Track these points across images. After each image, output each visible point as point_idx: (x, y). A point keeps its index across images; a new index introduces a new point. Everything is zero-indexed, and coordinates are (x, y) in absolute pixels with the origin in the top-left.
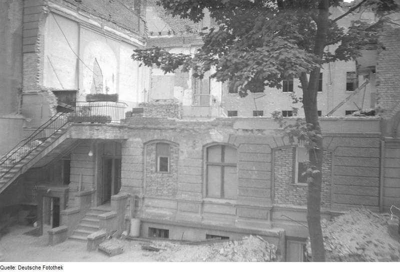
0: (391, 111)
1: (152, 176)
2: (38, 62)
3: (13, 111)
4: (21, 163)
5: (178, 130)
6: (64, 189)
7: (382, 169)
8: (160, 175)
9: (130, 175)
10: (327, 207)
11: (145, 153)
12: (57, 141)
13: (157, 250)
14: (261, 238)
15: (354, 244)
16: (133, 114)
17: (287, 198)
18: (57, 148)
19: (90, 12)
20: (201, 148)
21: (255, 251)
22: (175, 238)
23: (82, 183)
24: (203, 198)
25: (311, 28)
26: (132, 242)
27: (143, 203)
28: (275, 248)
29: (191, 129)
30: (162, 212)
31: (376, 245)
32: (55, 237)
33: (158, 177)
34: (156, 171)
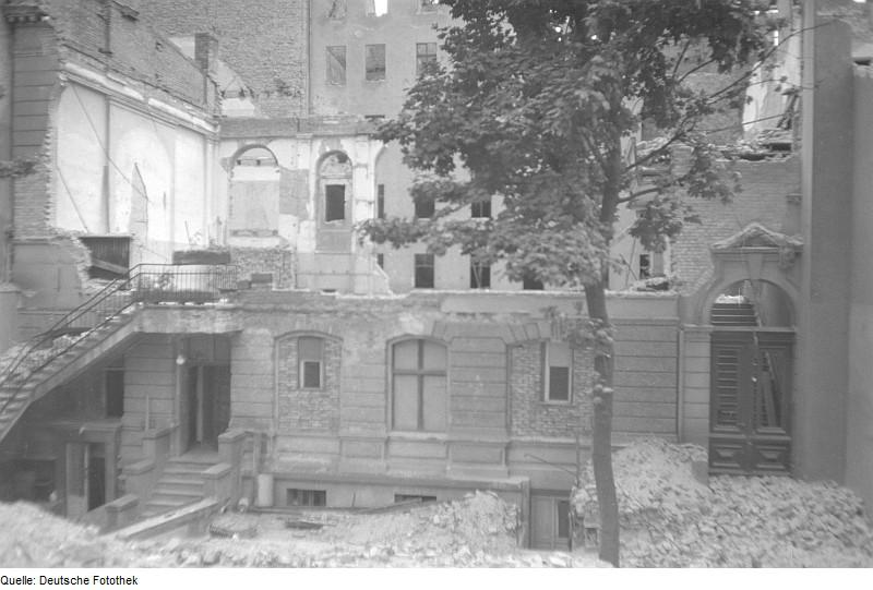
0: (693, 284)
4: (32, 381)
5: (341, 314)
6: (115, 425)
7: (681, 374)
8: (306, 394)
12: (111, 339)
13: (318, 527)
14: (494, 494)
15: (646, 494)
16: (253, 285)
17: (533, 425)
19: (125, 72)
21: (491, 515)
22: (338, 503)
24: (387, 431)
26: (264, 516)
29: (365, 312)
30: (311, 459)
31: (677, 494)
32: (120, 516)
33: (301, 398)
34: (298, 387)
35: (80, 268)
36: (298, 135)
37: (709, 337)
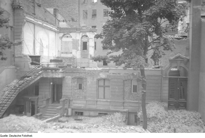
0: (165, 67)
1: (76, 91)
4: (19, 88)
6: (37, 97)
7: (162, 87)
8: (79, 91)
11: (73, 82)
12: (36, 79)
13: (82, 120)
16: (67, 67)
20: (96, 80)
21: (120, 118)
22: (86, 115)
23: (45, 95)
24: (97, 99)
25: (117, 8)
26: (70, 117)
30: (80, 105)
31: (161, 113)
34: (77, 89)
35: (29, 63)
36: (77, 31)
37: (168, 79)
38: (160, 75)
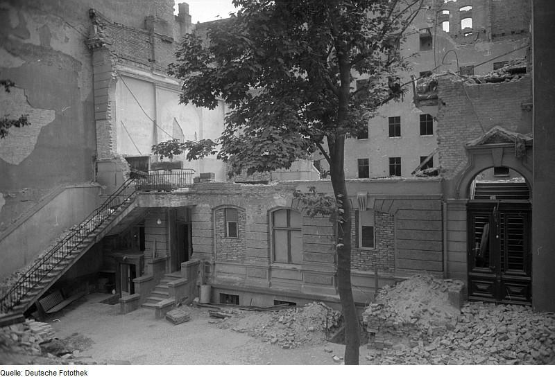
0: (453, 171)
2: (110, 129)
3: (89, 179)
6: (138, 256)
9: (200, 242)
10: (391, 272)
12: (126, 210)
15: (409, 313)
16: (201, 180)
18: (128, 216)
24: (270, 263)
26: (202, 309)
27: (214, 269)
28: (338, 315)
30: (232, 278)
35: (124, 173)
37: (465, 207)
38: (439, 196)
